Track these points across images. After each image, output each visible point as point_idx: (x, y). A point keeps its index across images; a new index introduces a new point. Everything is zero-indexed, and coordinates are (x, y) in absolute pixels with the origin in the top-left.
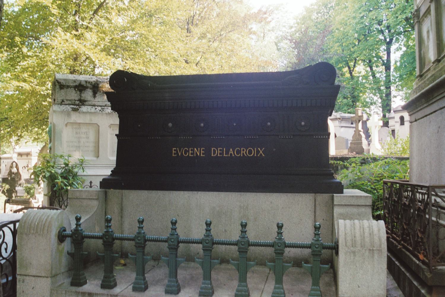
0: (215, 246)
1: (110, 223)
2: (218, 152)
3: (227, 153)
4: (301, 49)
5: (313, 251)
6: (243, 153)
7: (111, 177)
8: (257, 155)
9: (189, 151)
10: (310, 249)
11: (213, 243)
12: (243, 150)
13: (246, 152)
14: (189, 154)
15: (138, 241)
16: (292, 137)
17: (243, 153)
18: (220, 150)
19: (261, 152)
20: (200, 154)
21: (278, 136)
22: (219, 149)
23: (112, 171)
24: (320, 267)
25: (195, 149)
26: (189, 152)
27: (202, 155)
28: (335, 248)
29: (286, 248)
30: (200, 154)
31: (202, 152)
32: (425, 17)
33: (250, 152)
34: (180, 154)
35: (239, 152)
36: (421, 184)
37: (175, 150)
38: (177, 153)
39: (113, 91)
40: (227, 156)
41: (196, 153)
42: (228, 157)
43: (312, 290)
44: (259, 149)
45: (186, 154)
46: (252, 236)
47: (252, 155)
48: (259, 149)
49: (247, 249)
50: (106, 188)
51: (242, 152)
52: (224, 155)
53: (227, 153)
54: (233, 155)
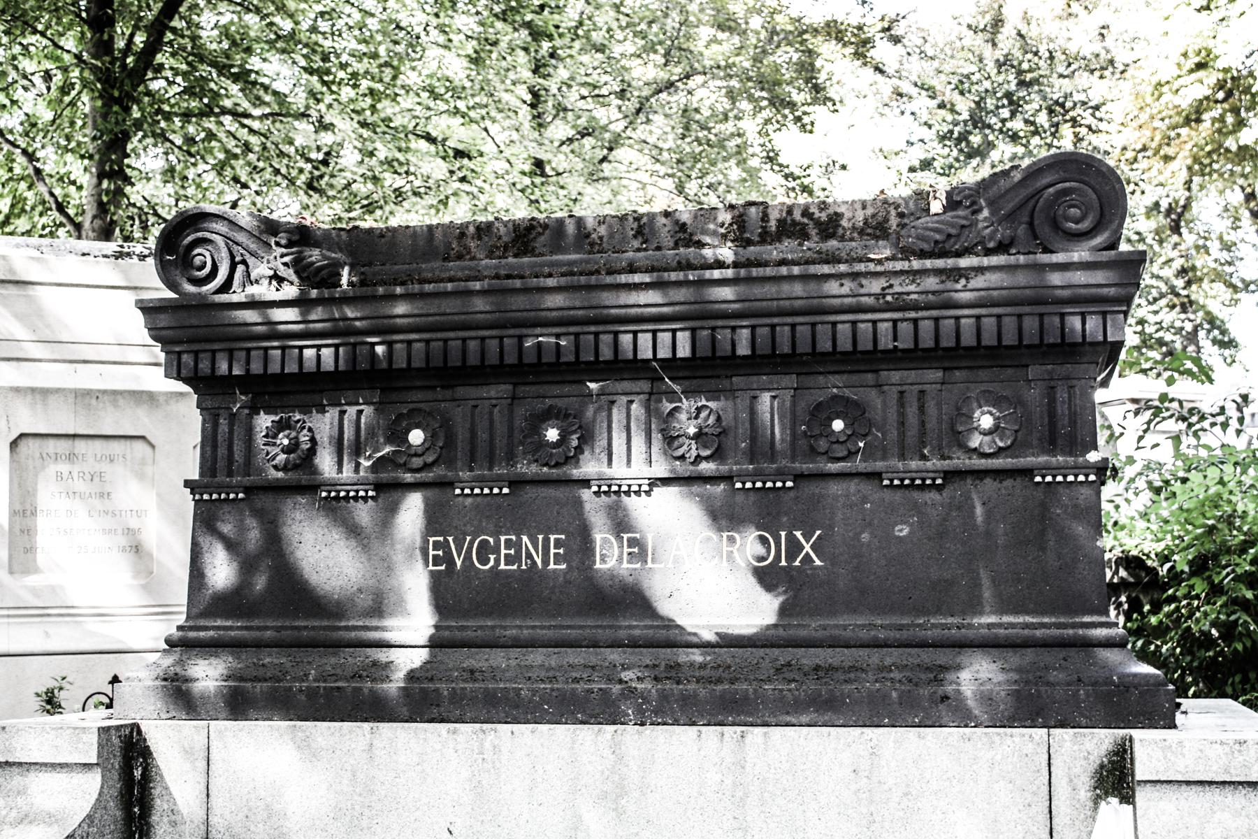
4: (341, 74)
8: (791, 557)
9: (496, 550)
14: (497, 561)
18: (509, 544)
19: (807, 548)
20: (546, 562)
21: (878, 476)
25: (525, 538)
26: (498, 552)
30: (546, 562)
31: (552, 551)
34: (459, 563)
41: (529, 556)
44: (798, 534)
45: (484, 561)
47: (487, 567)
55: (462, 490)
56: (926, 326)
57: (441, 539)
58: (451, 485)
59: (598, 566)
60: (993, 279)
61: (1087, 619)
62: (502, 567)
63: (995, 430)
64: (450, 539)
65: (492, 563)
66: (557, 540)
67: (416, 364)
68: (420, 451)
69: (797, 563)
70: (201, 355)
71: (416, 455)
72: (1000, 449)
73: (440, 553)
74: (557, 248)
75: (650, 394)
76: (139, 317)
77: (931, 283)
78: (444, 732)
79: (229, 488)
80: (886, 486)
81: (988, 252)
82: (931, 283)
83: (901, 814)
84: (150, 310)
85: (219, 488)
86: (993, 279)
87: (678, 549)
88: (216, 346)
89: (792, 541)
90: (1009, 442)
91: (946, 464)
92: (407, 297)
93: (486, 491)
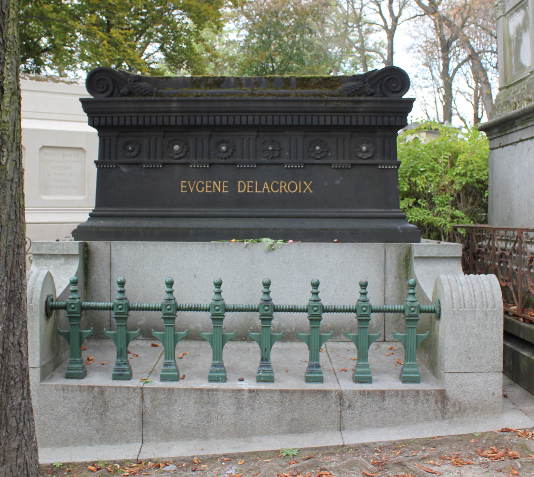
0: (131, 313)
3: (260, 188)
5: (165, 314)
6: (283, 188)
8: (302, 190)
9: (204, 186)
10: (355, 314)
11: (130, 309)
12: (283, 184)
13: (287, 187)
14: (205, 190)
17: (283, 188)
19: (308, 187)
20: (221, 190)
22: (248, 182)
23: (90, 215)
24: (417, 337)
25: (214, 182)
27: (223, 191)
28: (436, 313)
29: (323, 314)
30: (221, 190)
31: (224, 186)
32: (516, 11)
33: (293, 187)
35: (276, 187)
36: (505, 227)
37: (184, 184)
39: (92, 97)
40: (260, 192)
41: (216, 188)
42: (262, 193)
43: (357, 366)
44: (305, 183)
45: (200, 189)
48: (305, 183)
49: (175, 315)
51: (281, 187)
52: (256, 191)
53: (260, 188)
54: (269, 191)
57: (252, 182)
58: (189, 164)
59: (239, 191)
60: (370, 105)
61: (394, 210)
62: (248, 191)
63: (367, 151)
64: (189, 182)
65: (203, 190)
66: (250, 183)
67: (178, 123)
68: (178, 153)
69: (304, 192)
70: (101, 118)
71: (177, 154)
74: (228, 87)
75: (304, 136)
76: (80, 104)
77: (350, 105)
79: (156, 163)
80: (286, 168)
81: (368, 95)
82: (350, 105)
84: (84, 101)
85: (107, 164)
86: (370, 105)
88: (107, 115)
91: (352, 162)
92: (178, 101)
93: (201, 166)
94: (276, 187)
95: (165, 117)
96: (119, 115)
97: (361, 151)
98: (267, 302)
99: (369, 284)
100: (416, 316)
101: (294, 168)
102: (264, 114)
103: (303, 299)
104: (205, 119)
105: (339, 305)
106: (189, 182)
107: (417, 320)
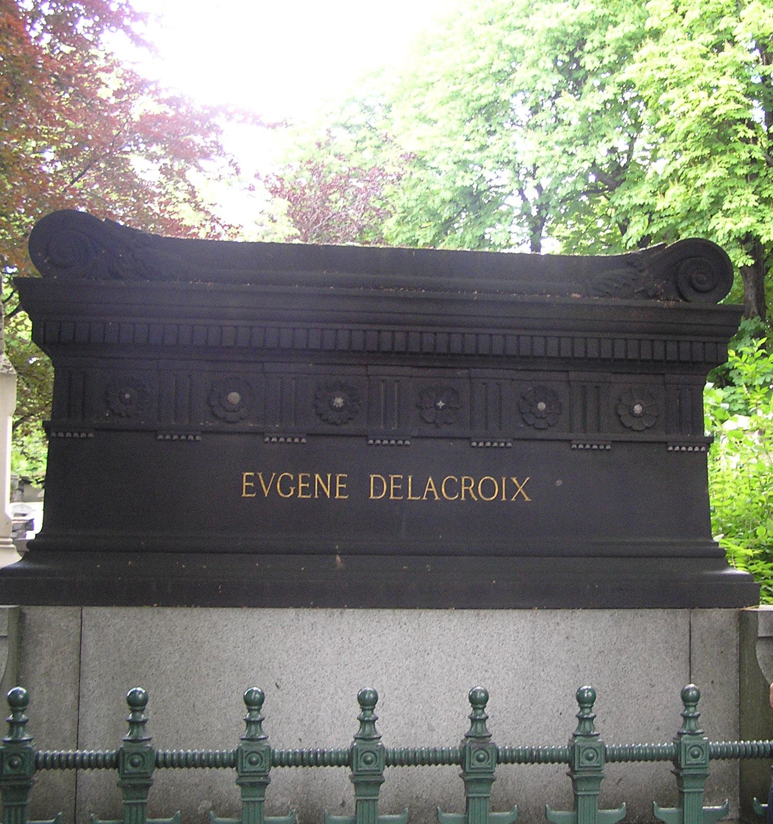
1: (142, 711)
2: (390, 487)
6: (467, 491)
7: (18, 566)
8: (509, 496)
12: (468, 483)
13: (475, 489)
14: (296, 491)
15: (248, 767)
16: (608, 447)
17: (467, 491)
20: (333, 493)
21: (569, 441)
25: (317, 476)
30: (333, 493)
31: (338, 486)
33: (488, 489)
35: (453, 488)
37: (249, 479)
38: (258, 489)
44: (514, 480)
46: (391, 735)
47: (292, 493)
50: (21, 603)
51: (463, 488)
55: (271, 438)
56: (400, 337)
58: (263, 435)
64: (260, 475)
72: (647, 428)
73: (252, 484)
78: (529, 615)
83: (597, 665)
87: (430, 487)
89: (509, 482)
90: (652, 424)
93: (76, 435)
94: (453, 488)
95: (535, 339)
96: (437, 329)
97: (632, 414)
98: (478, 736)
99: (150, 698)
100: (703, 766)
101: (491, 447)
102: (700, 338)
103: (449, 733)
104: (672, 347)
105: (423, 743)
106: (260, 475)
107: (706, 776)
